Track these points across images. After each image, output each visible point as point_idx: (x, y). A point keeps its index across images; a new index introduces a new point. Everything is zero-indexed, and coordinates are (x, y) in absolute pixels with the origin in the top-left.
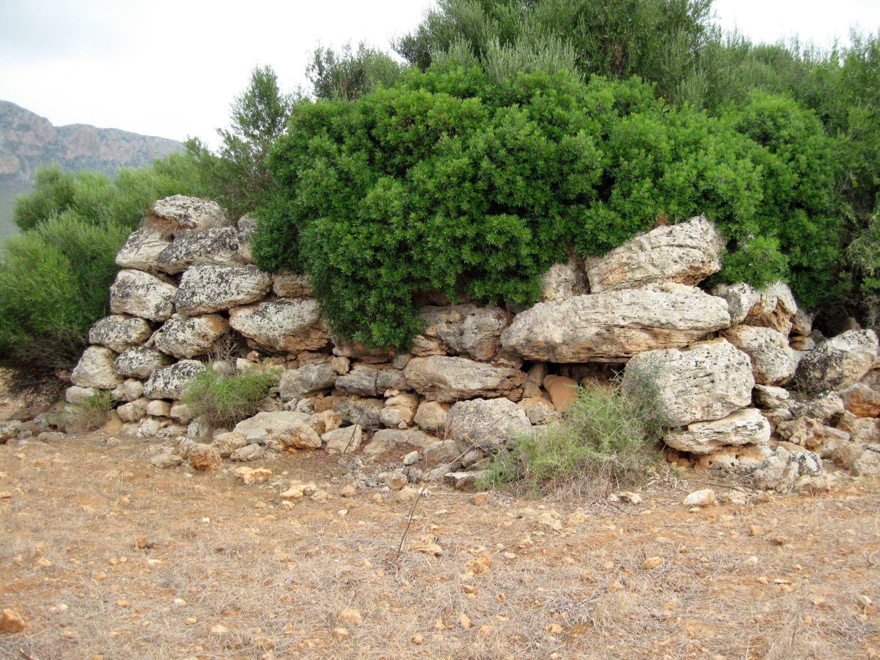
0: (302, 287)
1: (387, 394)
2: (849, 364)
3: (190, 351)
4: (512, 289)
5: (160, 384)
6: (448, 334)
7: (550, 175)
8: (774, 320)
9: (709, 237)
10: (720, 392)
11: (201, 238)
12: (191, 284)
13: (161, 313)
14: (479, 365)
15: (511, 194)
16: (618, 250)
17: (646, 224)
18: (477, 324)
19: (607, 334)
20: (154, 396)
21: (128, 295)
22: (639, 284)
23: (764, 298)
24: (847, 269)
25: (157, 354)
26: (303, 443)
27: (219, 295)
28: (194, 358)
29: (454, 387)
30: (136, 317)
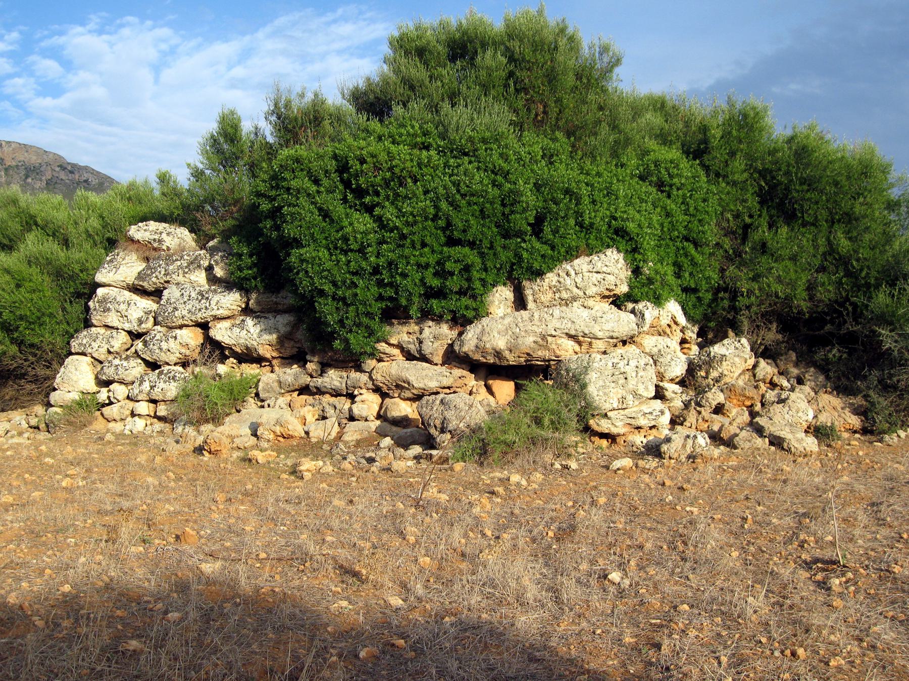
0: (276, 303)
1: (356, 393)
3: (173, 358)
5: (146, 386)
6: (409, 342)
7: (495, 215)
8: (668, 330)
9: (620, 265)
10: (631, 386)
11: (177, 260)
12: (173, 300)
13: (143, 326)
14: (435, 367)
15: (464, 231)
16: (548, 275)
17: (571, 254)
18: (437, 336)
19: (541, 342)
20: (139, 398)
21: (109, 310)
22: (566, 303)
23: (661, 313)
24: (725, 290)
25: (140, 361)
26: (291, 433)
27: (200, 310)
28: (175, 365)
29: (415, 385)
30: (117, 329)
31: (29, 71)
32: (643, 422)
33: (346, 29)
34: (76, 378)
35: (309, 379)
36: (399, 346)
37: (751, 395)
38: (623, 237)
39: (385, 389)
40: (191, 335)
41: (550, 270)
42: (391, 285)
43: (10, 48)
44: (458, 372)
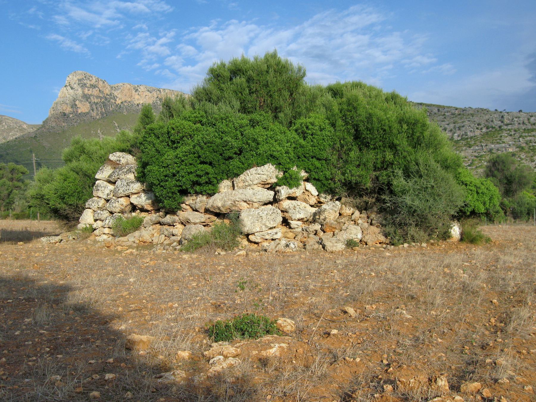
3: (117, 210)
4: (209, 187)
5: (107, 221)
16: (241, 175)
17: (249, 167)
18: (201, 201)
21: (98, 190)
31: (178, 52)
33: (355, 19)
34: (87, 218)
35: (161, 219)
36: (189, 205)
39: (184, 223)
40: (125, 200)
41: (242, 173)
42: (179, 180)
43: (169, 41)
44: (208, 216)
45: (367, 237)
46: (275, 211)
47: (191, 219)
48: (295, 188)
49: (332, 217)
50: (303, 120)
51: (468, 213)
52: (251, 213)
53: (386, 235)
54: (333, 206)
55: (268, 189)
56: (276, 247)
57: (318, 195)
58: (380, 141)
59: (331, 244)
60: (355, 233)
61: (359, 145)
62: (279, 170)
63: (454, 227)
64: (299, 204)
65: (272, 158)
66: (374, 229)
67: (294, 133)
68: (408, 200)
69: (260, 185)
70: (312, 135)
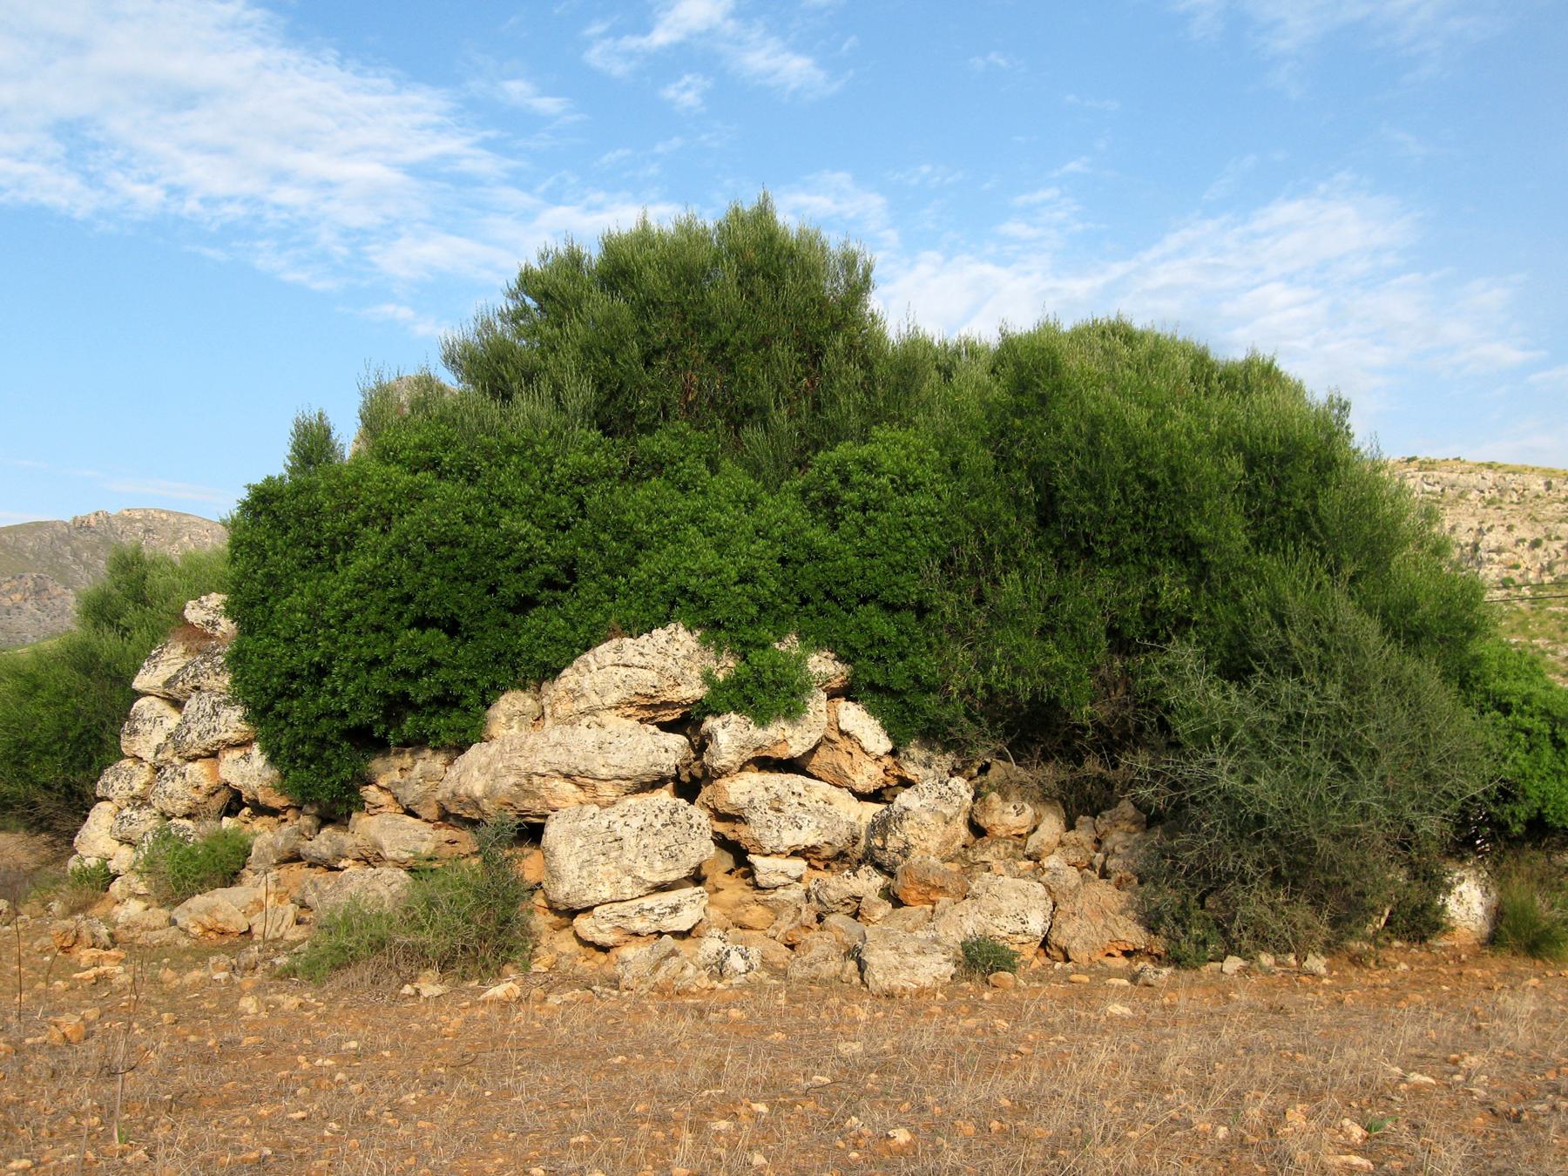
2: (912, 827)
4: (452, 719)
13: (160, 756)
16: (566, 672)
32: (638, 925)
37: (939, 884)
38: (692, 601)
40: (205, 771)
41: (569, 663)
44: (445, 834)
45: (1068, 930)
46: (681, 816)
47: (385, 843)
48: (783, 724)
49: (933, 843)
50: (842, 450)
51: (1517, 829)
52: (584, 825)
53: (1151, 922)
54: (941, 797)
55: (666, 727)
56: (657, 968)
57: (893, 753)
58: (1135, 529)
59: (892, 958)
60: (1013, 907)
61: (1058, 550)
62: (719, 650)
63: (1463, 887)
64: (799, 789)
65: (675, 603)
66: (1104, 892)
67: (791, 499)
68: (1225, 773)
69: (631, 711)
70: (864, 509)
